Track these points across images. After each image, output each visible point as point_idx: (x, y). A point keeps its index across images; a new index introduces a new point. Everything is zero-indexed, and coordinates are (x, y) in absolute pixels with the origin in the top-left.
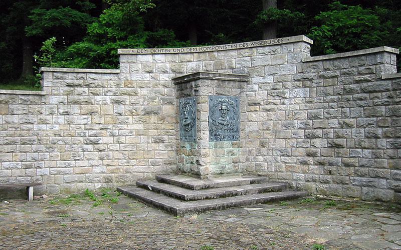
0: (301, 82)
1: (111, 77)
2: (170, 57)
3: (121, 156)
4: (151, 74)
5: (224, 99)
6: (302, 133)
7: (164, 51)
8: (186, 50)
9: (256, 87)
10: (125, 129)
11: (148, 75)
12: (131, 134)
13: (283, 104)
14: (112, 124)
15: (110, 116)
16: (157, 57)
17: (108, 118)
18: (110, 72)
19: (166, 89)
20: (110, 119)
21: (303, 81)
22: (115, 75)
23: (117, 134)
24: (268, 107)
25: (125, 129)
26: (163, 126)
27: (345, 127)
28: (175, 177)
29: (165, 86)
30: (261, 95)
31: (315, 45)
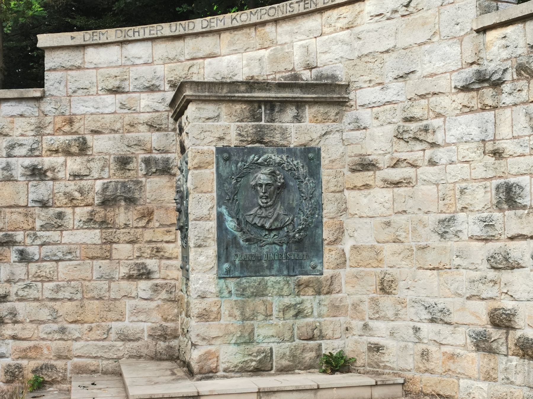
0: (474, 94)
1: (22, 108)
2: (162, 49)
3: (44, 314)
4: (118, 96)
5: (265, 156)
6: (480, 251)
7: (147, 31)
8: (198, 24)
9: (366, 115)
10: (55, 243)
11: (110, 98)
12: (69, 257)
13: (432, 163)
14: (25, 230)
15: (20, 210)
16: (133, 50)
17: (14, 216)
18: (16, 96)
19: (156, 135)
20: (21, 218)
21: (478, 90)
22: (32, 104)
23: (37, 258)
24: (396, 174)
25: (55, 243)
26: (148, 235)
27: (258, 211)
28: (89, 362)
29: (152, 126)
30: (378, 141)
31: (34, 36)
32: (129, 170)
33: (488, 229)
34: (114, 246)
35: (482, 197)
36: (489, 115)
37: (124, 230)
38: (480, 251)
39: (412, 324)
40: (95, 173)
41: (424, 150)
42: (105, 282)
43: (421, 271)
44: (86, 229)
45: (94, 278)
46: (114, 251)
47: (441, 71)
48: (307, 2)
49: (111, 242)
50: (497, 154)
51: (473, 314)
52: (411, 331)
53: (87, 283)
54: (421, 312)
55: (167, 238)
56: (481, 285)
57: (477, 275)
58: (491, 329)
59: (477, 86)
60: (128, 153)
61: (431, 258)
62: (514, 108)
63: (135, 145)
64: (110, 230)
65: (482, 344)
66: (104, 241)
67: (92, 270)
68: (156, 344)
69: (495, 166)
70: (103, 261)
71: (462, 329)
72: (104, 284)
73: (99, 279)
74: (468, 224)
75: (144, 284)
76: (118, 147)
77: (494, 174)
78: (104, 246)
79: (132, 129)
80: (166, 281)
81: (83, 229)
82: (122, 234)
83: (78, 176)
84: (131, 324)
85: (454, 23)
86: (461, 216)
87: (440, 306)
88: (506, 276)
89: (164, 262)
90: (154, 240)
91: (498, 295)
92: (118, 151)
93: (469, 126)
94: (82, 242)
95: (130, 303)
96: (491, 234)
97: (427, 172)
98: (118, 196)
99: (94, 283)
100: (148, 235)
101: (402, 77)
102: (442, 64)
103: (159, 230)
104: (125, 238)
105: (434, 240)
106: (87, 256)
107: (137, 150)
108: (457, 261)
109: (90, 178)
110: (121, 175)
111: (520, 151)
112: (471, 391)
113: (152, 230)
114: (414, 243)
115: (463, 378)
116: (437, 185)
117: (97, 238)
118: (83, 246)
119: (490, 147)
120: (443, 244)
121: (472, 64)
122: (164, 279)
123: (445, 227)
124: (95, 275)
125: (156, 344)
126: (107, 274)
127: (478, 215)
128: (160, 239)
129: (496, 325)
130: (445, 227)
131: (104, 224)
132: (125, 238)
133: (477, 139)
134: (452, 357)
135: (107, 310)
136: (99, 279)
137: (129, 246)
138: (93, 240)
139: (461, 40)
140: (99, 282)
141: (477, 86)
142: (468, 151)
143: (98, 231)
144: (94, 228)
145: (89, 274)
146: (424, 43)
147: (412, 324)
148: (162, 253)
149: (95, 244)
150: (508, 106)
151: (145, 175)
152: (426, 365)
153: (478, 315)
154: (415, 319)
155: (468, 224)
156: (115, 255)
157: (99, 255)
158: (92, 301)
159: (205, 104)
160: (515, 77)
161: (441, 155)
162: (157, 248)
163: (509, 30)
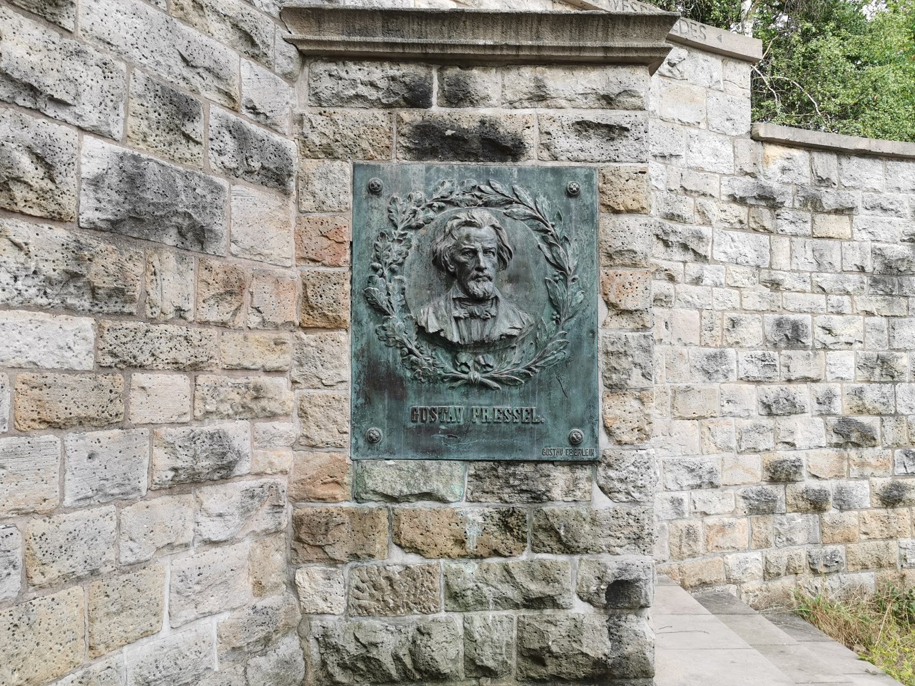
6: (751, 395)
26: (230, 348)
32: (188, 138)
33: (767, 369)
34: (139, 378)
35: (754, 331)
36: (765, 238)
37: (172, 329)
38: (751, 395)
39: (668, 495)
40: (88, 108)
41: (685, 262)
42: (104, 509)
43: (678, 421)
44: (40, 308)
45: (68, 501)
46: (137, 397)
47: (712, 169)
48: (889, 2)
49: (130, 366)
50: (775, 285)
51: (747, 471)
52: (668, 506)
53: (38, 525)
54: (682, 477)
55: (273, 361)
56: (757, 435)
57: (747, 423)
58: (770, 488)
59: (753, 202)
60: (182, 84)
61: (694, 405)
62: (793, 239)
63: (208, 69)
64: (131, 324)
65: (761, 507)
66: (109, 360)
67: (63, 471)
68: (245, 671)
69: (771, 298)
70: (101, 434)
71: (731, 491)
72: (102, 518)
73: (84, 501)
74: (739, 361)
75: (216, 498)
76: (162, 54)
77: (768, 307)
78: (105, 381)
79: (194, 17)
80: (264, 480)
81: (28, 308)
82: (165, 340)
83: (33, 91)
84: (179, 635)
85: (725, 117)
86: (731, 352)
87: (707, 467)
88: (786, 423)
89: (262, 425)
90: (246, 364)
91: (773, 445)
92: (158, 63)
93: (747, 245)
94: (22, 361)
95: (169, 567)
96: (769, 376)
97: (684, 289)
98: (176, 213)
99: (72, 521)
100: (230, 348)
101: (664, 157)
102: (714, 161)
103: (257, 335)
104: (173, 354)
105: (698, 380)
106: (45, 415)
107: (207, 88)
108: (728, 408)
109: (70, 119)
110: (161, 147)
111: (799, 286)
112: (747, 565)
113: (239, 336)
114: (669, 384)
115: (729, 553)
116: (700, 310)
117: (82, 348)
118: (27, 376)
119: (765, 275)
120: (708, 386)
121: (747, 174)
122: (259, 474)
123: (713, 366)
124: (74, 487)
125: (245, 671)
126: (119, 480)
127: (750, 353)
128: (259, 363)
129: (773, 480)
130: (713, 366)
131: (113, 300)
132: (173, 354)
133: (752, 264)
134: (722, 529)
135: (113, 609)
136: (84, 501)
137: (181, 381)
138: (69, 354)
139: (733, 139)
140: (85, 513)
141: (753, 202)
142: (741, 275)
143: (87, 322)
144: (70, 310)
145: (50, 490)
146: (689, 124)
147: (668, 495)
148: (264, 403)
149: (71, 371)
150: (786, 235)
151: (229, 172)
152: (694, 547)
153: (751, 472)
154: (672, 488)
155: (739, 361)
156: (140, 411)
157: (92, 413)
158: (63, 593)
159: (605, 68)
160: (797, 205)
161: (709, 272)
162: (257, 389)
163: (795, 153)
